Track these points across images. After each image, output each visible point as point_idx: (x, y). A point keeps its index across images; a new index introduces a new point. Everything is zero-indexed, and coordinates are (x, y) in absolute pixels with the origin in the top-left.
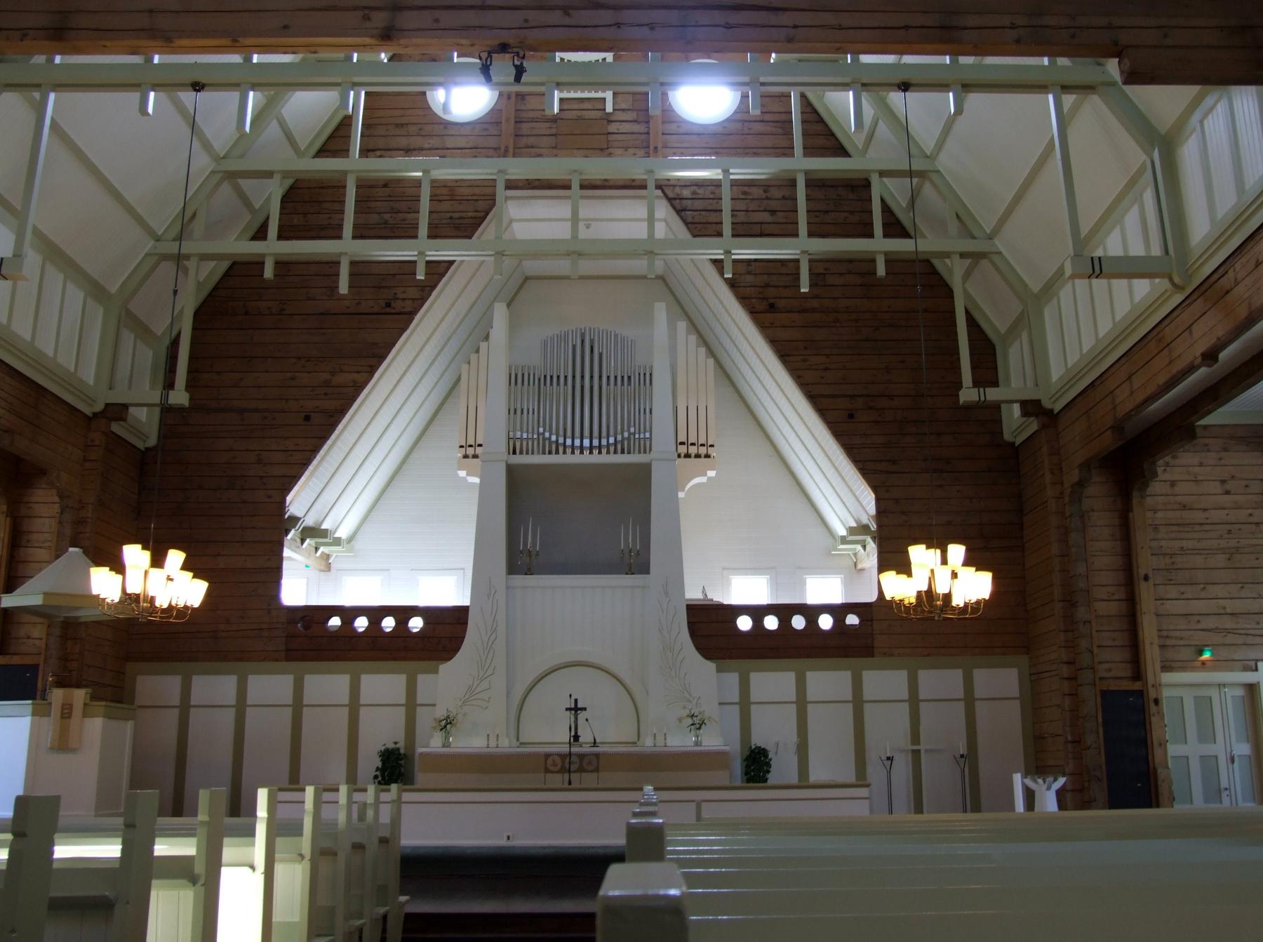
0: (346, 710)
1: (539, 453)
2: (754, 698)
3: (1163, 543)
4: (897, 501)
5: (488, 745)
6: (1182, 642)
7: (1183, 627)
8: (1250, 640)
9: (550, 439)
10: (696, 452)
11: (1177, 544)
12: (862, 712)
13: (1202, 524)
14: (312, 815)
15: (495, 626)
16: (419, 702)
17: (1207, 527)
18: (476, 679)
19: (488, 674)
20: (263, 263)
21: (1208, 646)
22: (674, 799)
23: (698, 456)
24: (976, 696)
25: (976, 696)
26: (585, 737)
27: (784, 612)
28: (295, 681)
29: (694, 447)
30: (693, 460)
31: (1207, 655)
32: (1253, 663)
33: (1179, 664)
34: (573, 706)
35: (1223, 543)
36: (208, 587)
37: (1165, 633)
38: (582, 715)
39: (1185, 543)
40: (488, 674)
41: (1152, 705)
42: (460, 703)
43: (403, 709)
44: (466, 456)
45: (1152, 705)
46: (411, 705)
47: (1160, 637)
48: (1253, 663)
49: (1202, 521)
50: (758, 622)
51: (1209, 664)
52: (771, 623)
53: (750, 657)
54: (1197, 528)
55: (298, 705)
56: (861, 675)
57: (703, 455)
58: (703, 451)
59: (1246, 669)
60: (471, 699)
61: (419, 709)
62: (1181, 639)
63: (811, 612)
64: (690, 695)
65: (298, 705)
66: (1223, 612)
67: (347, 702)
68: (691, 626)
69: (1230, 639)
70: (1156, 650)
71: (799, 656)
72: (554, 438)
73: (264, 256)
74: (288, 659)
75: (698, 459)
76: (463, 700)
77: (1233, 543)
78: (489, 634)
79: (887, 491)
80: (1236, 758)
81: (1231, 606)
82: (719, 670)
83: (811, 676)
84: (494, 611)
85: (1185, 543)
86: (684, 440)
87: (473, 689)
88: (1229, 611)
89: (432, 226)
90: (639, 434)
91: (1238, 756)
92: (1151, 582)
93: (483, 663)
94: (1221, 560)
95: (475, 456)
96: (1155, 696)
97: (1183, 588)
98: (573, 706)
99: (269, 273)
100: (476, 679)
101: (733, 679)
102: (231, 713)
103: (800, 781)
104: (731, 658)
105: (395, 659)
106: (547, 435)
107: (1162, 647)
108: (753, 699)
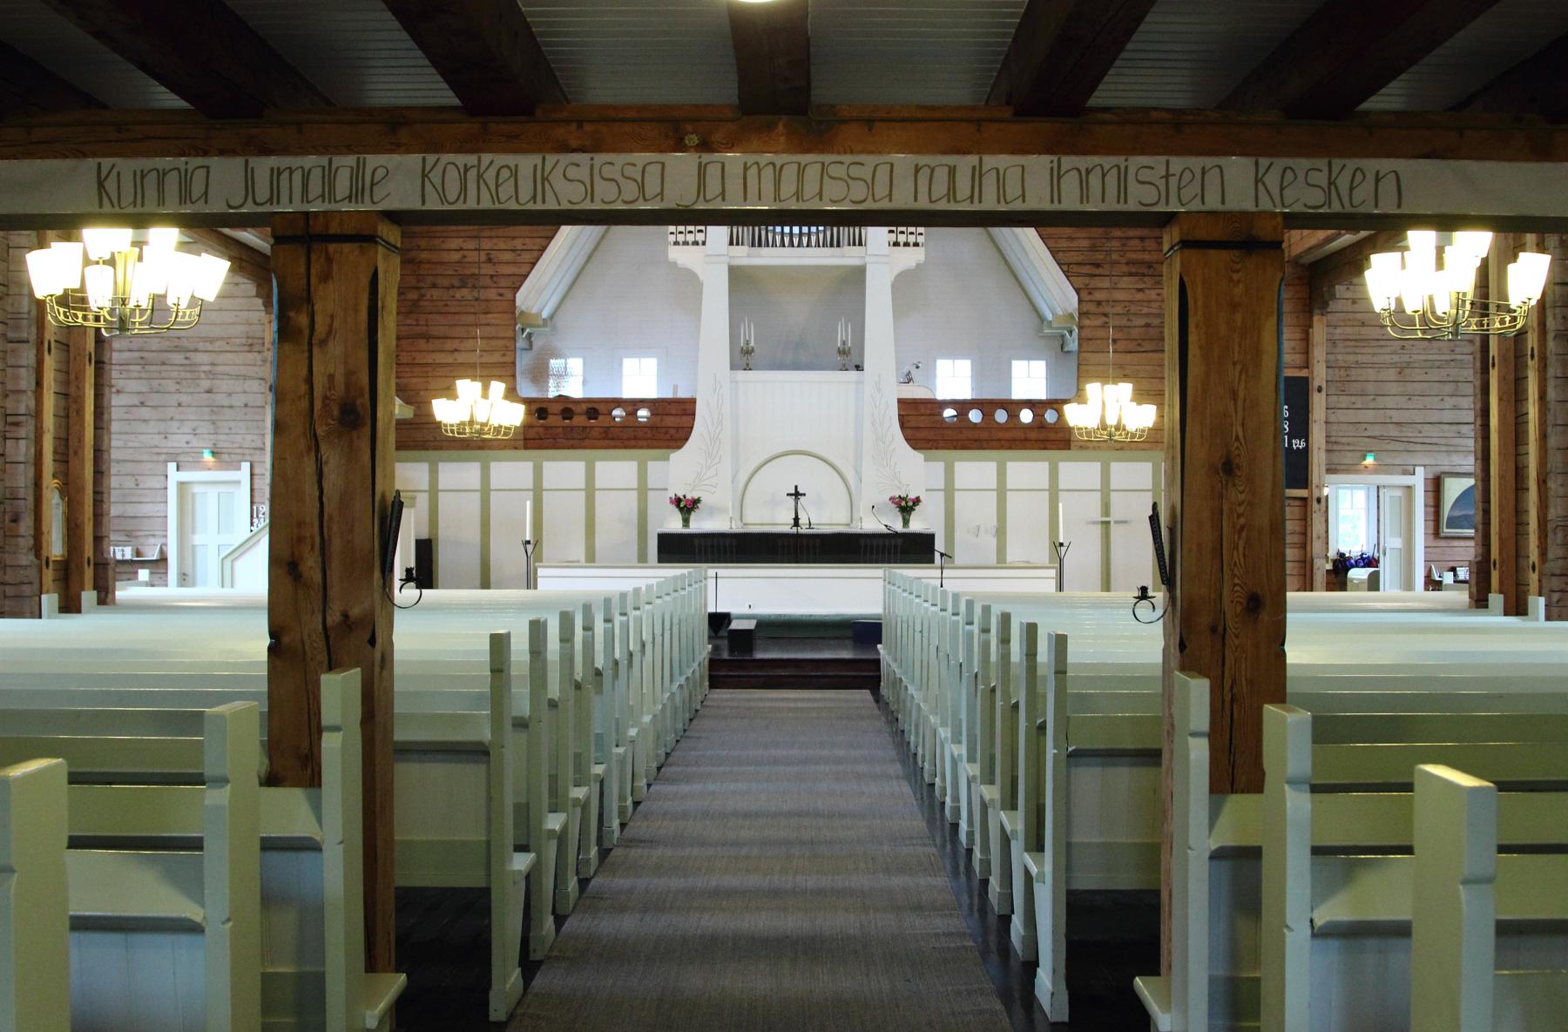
0: (478, 495)
2: (545, 485)
3: (1340, 357)
4: (1099, 303)
6: (1347, 448)
7: (1351, 434)
8: (1412, 447)
11: (1352, 358)
12: (541, 499)
13: (1378, 340)
14: (267, 612)
16: (597, 486)
17: (1382, 343)
21: (1371, 451)
23: (906, 244)
24: (650, 486)
25: (650, 486)
26: (803, 520)
27: (987, 406)
30: (901, 248)
31: (1370, 460)
32: (1411, 468)
33: (1343, 467)
35: (1396, 358)
36: (573, 357)
37: (1333, 439)
38: (802, 499)
39: (1359, 358)
41: (1315, 503)
44: (896, 244)
45: (1315, 503)
46: (643, 490)
47: (1327, 442)
48: (1411, 468)
49: (1380, 337)
50: (1038, 416)
51: (1371, 467)
52: (975, 416)
53: (955, 448)
54: (1375, 343)
55: (485, 491)
56: (953, 466)
57: (902, 244)
59: (1405, 473)
61: (440, 494)
62: (1349, 444)
63: (1013, 407)
65: (485, 491)
66: (1388, 421)
68: (902, 419)
69: (1393, 446)
70: (1323, 455)
71: (1001, 447)
75: (897, 248)
77: (1406, 358)
79: (1090, 293)
80: (51, 564)
81: (1397, 416)
82: (926, 460)
83: (600, 466)
85: (1359, 358)
88: (1394, 420)
91: (54, 561)
92: (1324, 393)
94: (1391, 374)
95: (916, 244)
96: (1318, 495)
97: (1353, 399)
101: (938, 468)
102: (477, 496)
104: (937, 448)
107: (1328, 451)
108: (957, 486)
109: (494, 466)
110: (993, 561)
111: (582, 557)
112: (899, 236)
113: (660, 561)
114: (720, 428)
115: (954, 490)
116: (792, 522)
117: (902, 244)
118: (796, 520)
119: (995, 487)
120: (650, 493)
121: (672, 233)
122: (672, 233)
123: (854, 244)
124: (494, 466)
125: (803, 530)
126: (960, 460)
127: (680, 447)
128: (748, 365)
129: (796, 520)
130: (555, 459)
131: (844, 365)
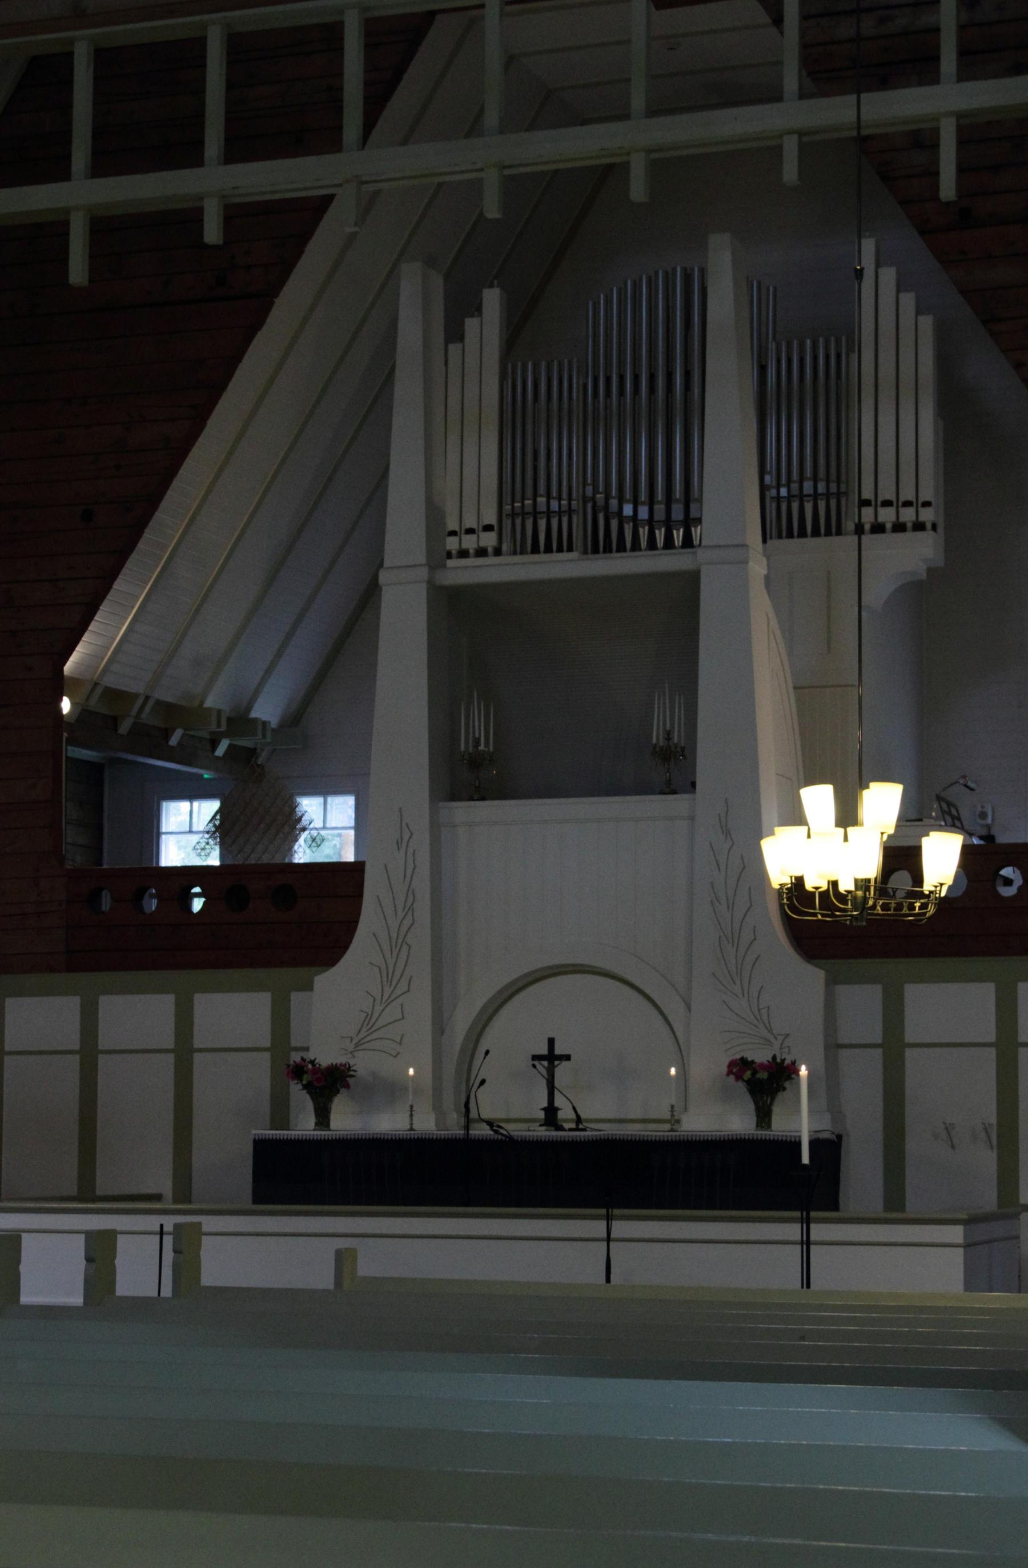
1: (780, 537)
2: (103, 1043)
5: (411, 1124)
9: (635, 517)
10: (914, 519)
15: (411, 900)
18: (378, 1001)
19: (398, 992)
20: (200, 211)
22: (384, 1231)
23: (899, 527)
26: (565, 1113)
28: (83, 1006)
29: (468, 526)
34: (558, 1051)
38: (562, 1071)
40: (398, 992)
42: (351, 1047)
43: (171, 1058)
57: (909, 525)
58: (908, 515)
60: (369, 1038)
61: (197, 1057)
64: (770, 1030)
67: (77, 1047)
72: (628, 510)
73: (67, 211)
74: (72, 967)
76: (355, 1042)
78: (400, 914)
84: (409, 875)
86: (891, 496)
87: (373, 1021)
89: (964, 53)
90: (523, 499)
93: (391, 971)
95: (919, 526)
98: (558, 1051)
99: (212, 233)
100: (378, 1001)
103: (1000, 1205)
105: (252, 965)
106: (628, 510)
108: (909, 1037)
109: (106, 1002)
110: (74, 1191)
111: (166, 1187)
112: (902, 510)
113: (256, 1200)
114: (407, 923)
115: (192, 1051)
116: (542, 1115)
117: (889, 526)
118: (551, 1111)
119: (992, 1038)
120: (102, 1059)
121: (927, 504)
122: (927, 504)
123: (790, 535)
124: (106, 1002)
125: (480, 1131)
126: (20, 993)
127: (332, 962)
128: (669, 782)
129: (551, 1111)
130: (218, 988)
131: (669, 782)
